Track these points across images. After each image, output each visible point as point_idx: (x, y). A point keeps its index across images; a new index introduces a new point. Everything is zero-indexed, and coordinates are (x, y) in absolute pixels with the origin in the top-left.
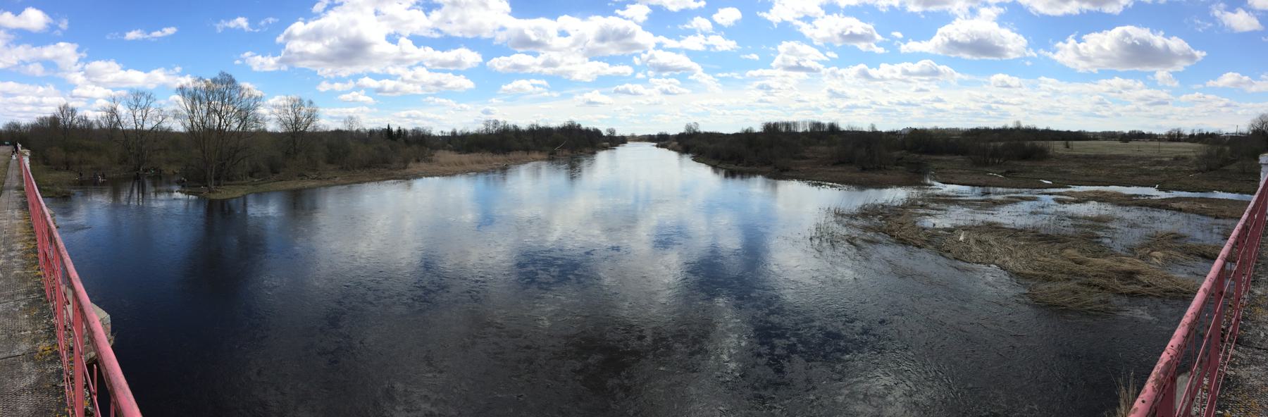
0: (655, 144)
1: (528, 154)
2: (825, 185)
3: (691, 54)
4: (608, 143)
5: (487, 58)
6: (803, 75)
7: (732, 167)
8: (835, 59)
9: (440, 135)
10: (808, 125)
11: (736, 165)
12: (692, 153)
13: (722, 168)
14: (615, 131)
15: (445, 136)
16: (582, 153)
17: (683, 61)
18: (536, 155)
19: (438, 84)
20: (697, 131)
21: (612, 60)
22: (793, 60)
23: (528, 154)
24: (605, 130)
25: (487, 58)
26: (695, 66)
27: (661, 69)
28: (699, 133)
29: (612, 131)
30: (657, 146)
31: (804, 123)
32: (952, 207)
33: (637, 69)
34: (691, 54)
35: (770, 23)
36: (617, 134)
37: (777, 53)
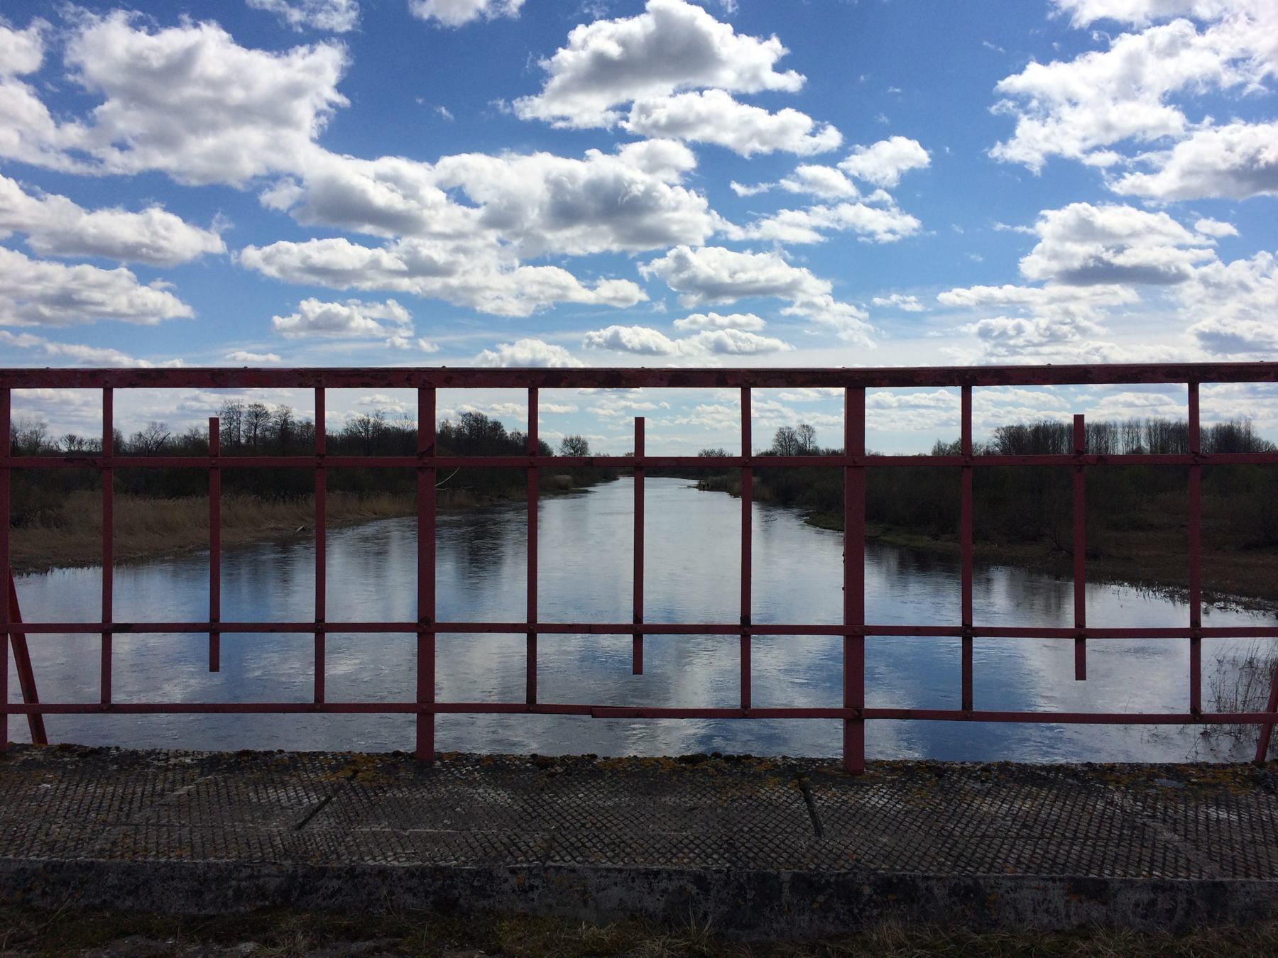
0: (695, 482)
1: (361, 499)
2: (1225, 600)
3: (797, 254)
4: (568, 477)
5: (235, 241)
6: (1124, 293)
7: (924, 542)
8: (1230, 238)
9: (64, 448)
10: (1143, 433)
11: (936, 537)
12: (799, 505)
13: (893, 545)
14: (585, 444)
15: (79, 452)
16: (502, 502)
17: (773, 270)
18: (384, 503)
19: (65, 300)
20: (810, 447)
21: (586, 268)
22: (1081, 252)
23: (361, 499)
24: (560, 444)
25: (235, 241)
26: (801, 274)
27: (713, 290)
28: (816, 452)
29: (577, 445)
30: (701, 488)
31: (1132, 427)
32: (115, 426)
33: (655, 287)
34: (797, 254)
35: (1019, 169)
36: (593, 451)
37: (1031, 242)
